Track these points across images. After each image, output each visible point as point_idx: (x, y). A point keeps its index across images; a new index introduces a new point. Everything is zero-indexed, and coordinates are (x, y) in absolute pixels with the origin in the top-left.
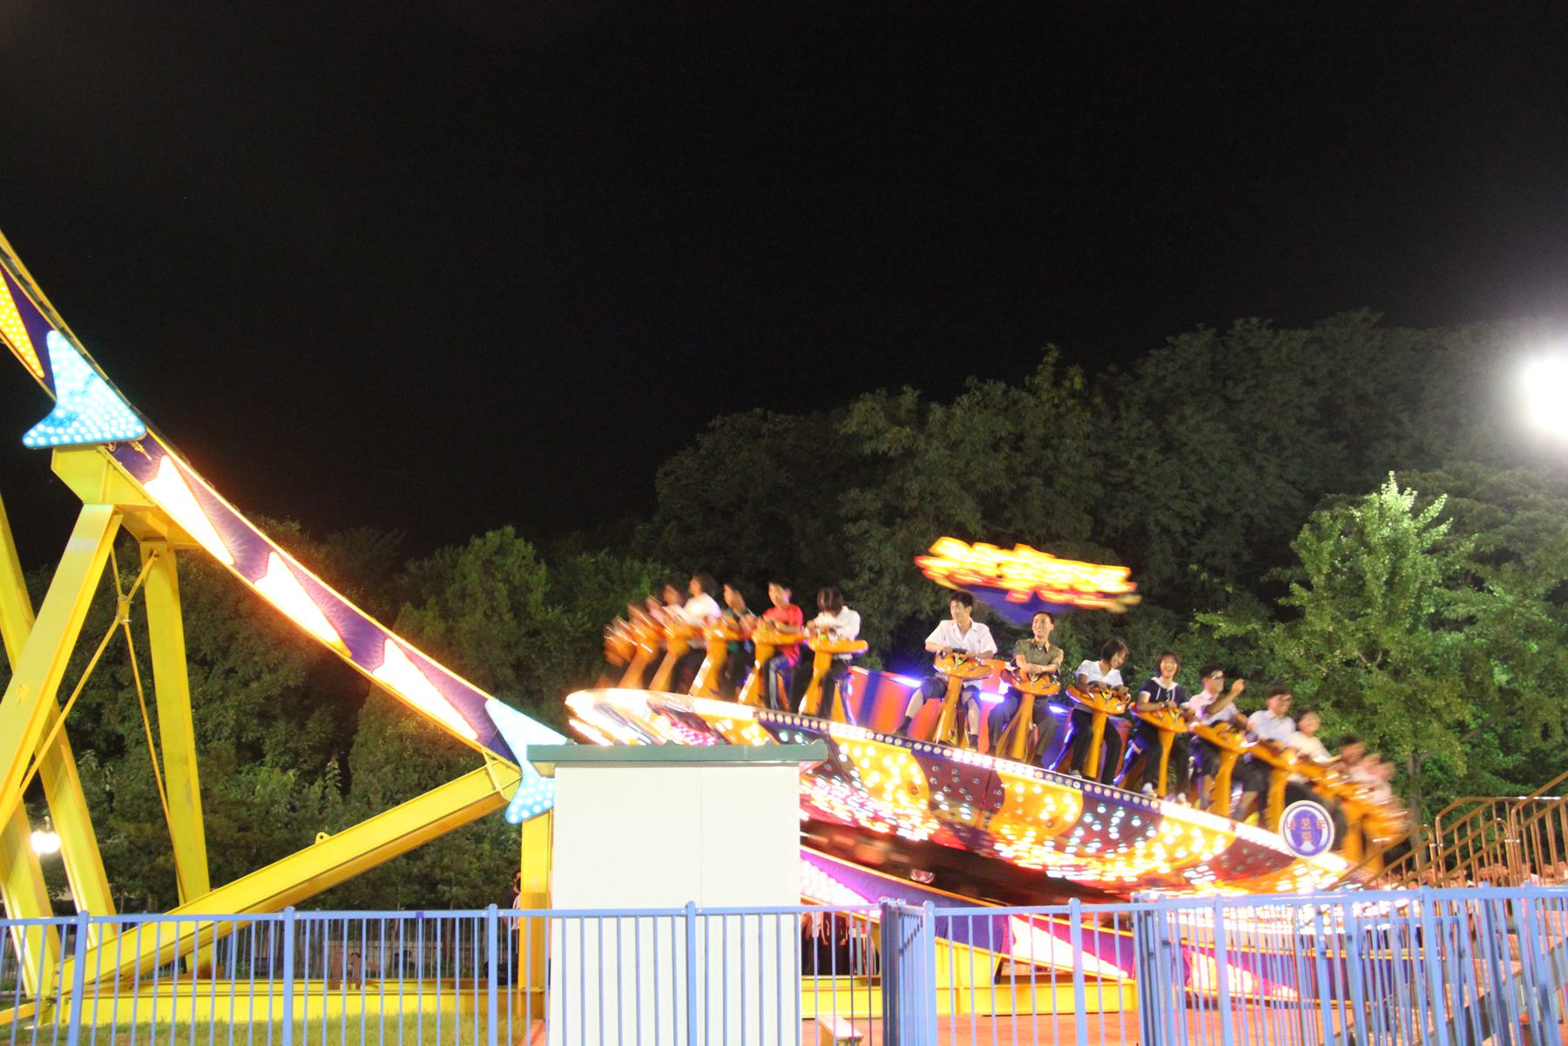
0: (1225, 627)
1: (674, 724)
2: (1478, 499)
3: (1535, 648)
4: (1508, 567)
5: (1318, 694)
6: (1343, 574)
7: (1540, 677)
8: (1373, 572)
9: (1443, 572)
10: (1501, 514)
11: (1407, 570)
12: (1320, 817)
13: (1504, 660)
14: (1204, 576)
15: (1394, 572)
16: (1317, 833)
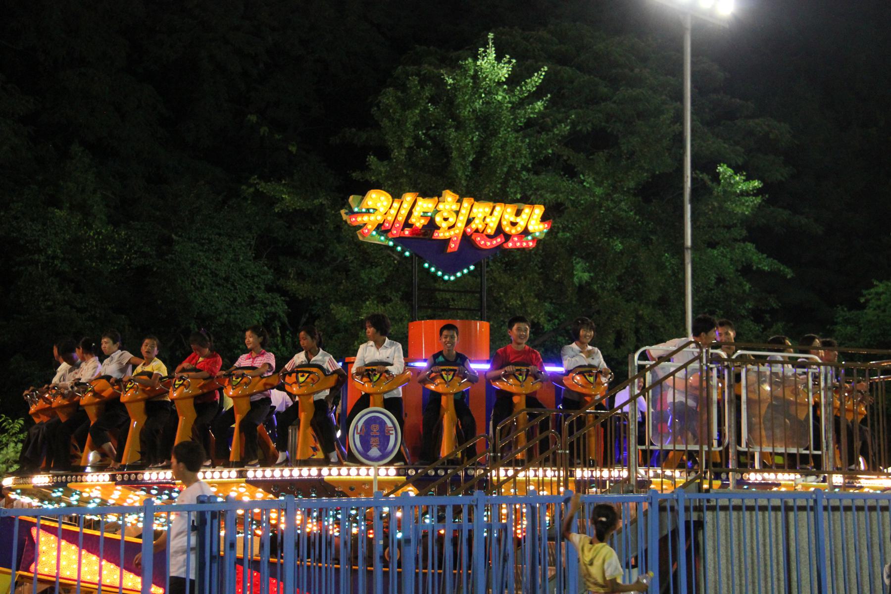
0: (288, 199)
1: (406, 414)
2: (580, 68)
3: (620, 247)
4: (601, 157)
5: (386, 284)
6: (426, 148)
7: (620, 278)
8: (459, 150)
9: (533, 156)
10: (604, 90)
11: (496, 151)
12: (389, 424)
13: (587, 258)
14: (264, 130)
15: (482, 151)
16: (384, 439)
